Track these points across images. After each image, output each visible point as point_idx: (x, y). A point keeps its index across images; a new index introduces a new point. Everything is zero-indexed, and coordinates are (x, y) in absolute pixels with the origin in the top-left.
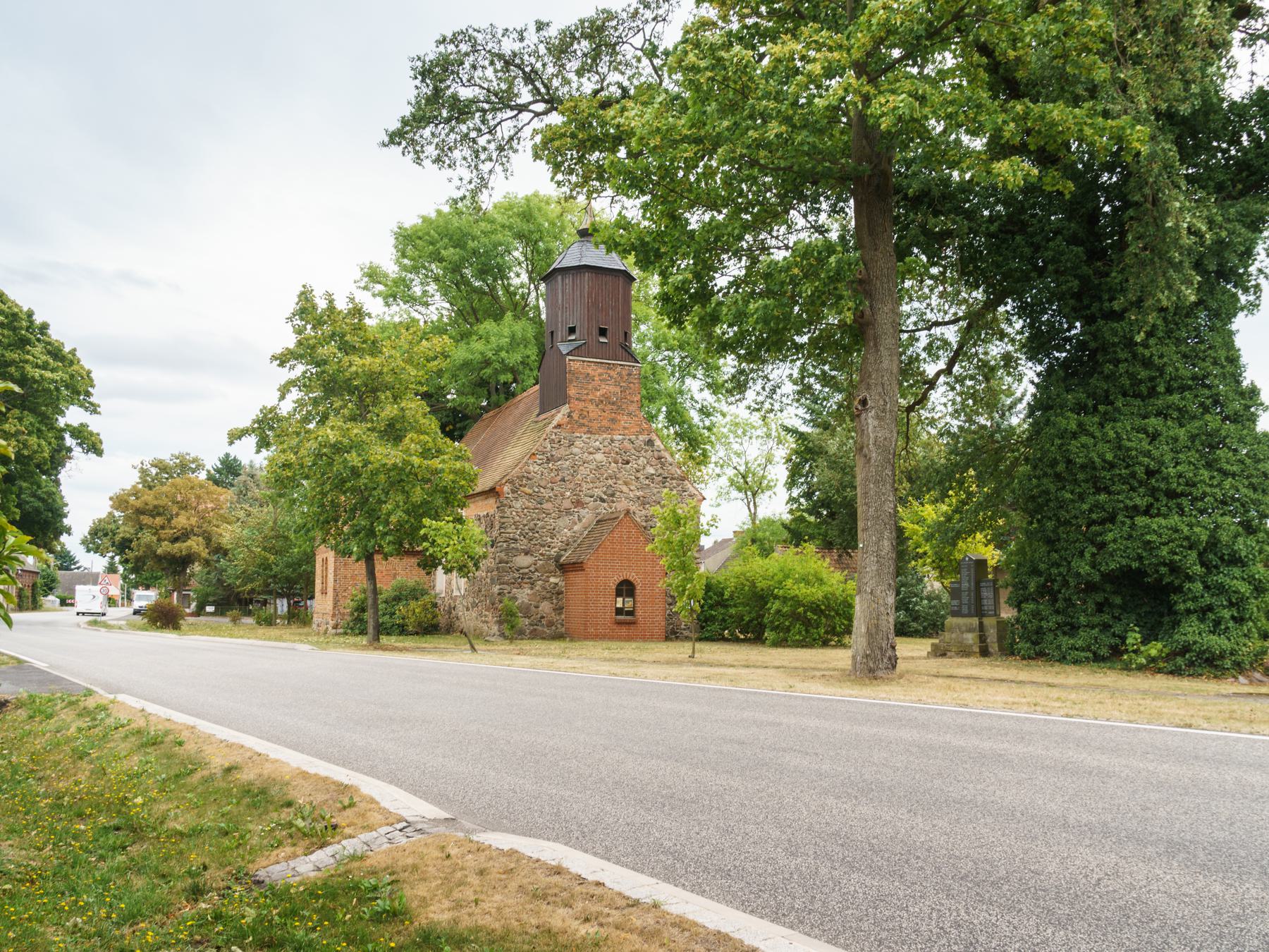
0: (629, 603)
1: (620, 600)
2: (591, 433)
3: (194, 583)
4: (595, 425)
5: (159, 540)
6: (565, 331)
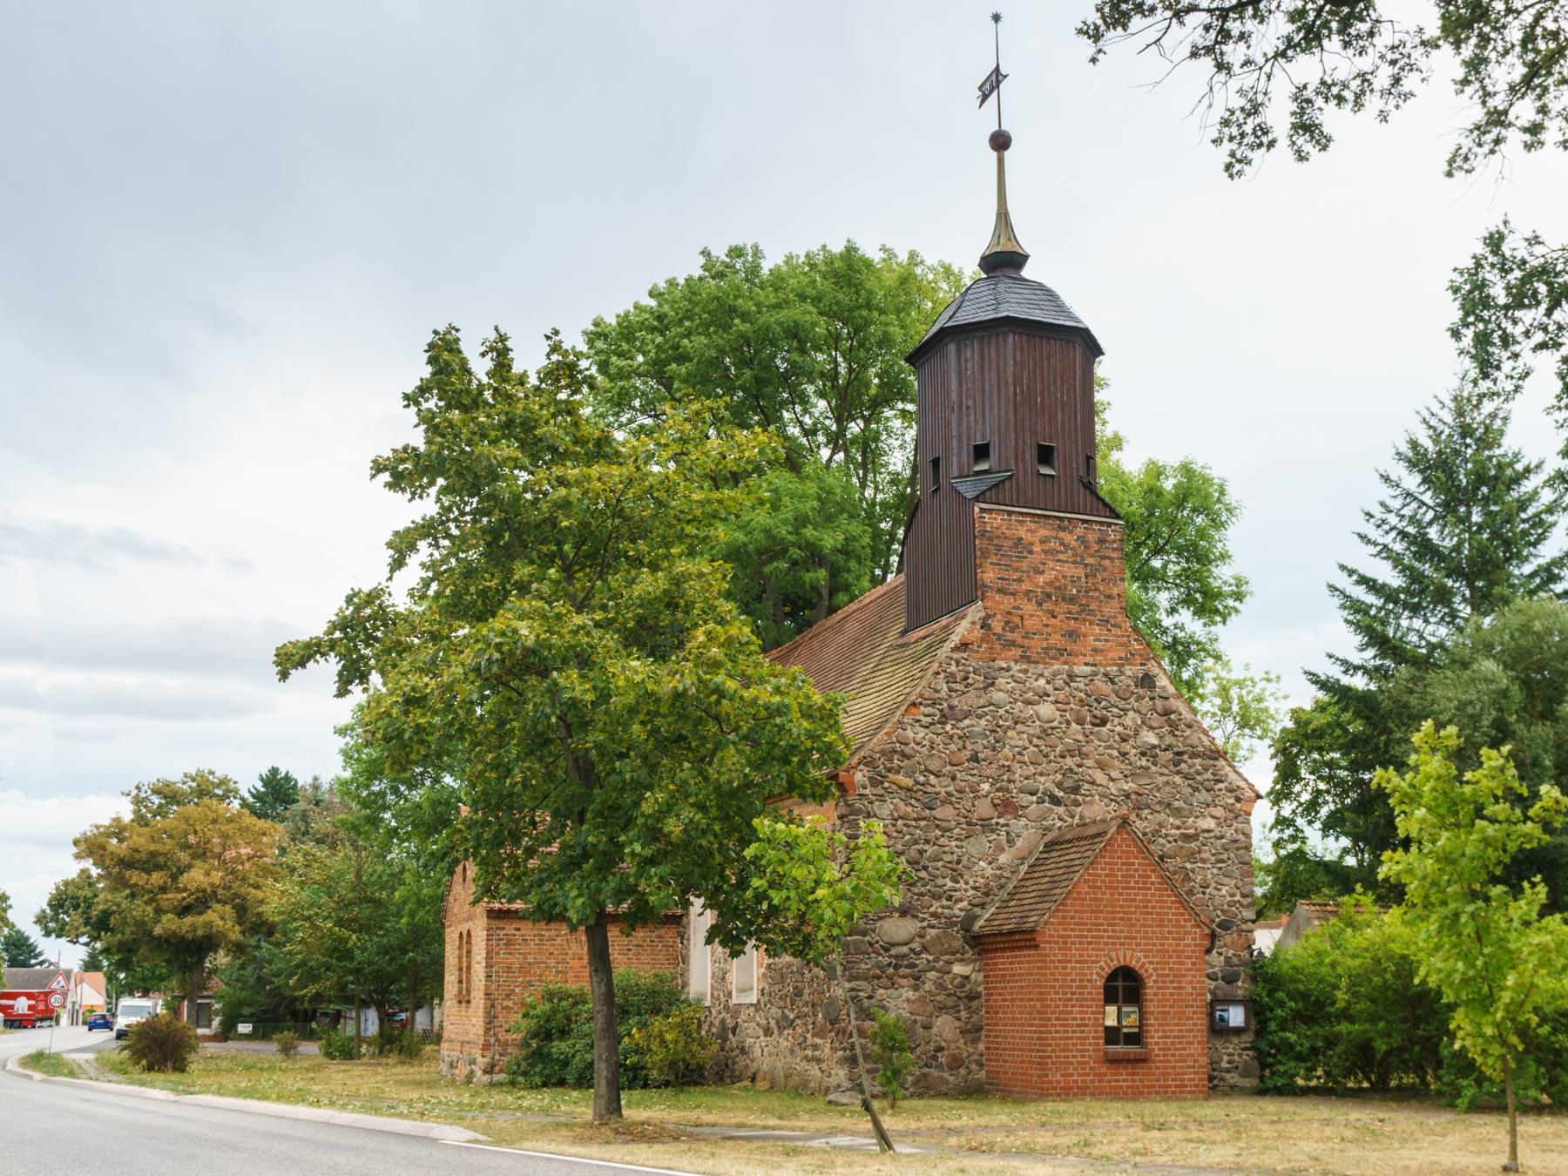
0: (1131, 1021)
1: (1112, 1010)
2: (1029, 660)
3: (217, 984)
4: (1037, 644)
5: (159, 911)
6: (967, 454)
